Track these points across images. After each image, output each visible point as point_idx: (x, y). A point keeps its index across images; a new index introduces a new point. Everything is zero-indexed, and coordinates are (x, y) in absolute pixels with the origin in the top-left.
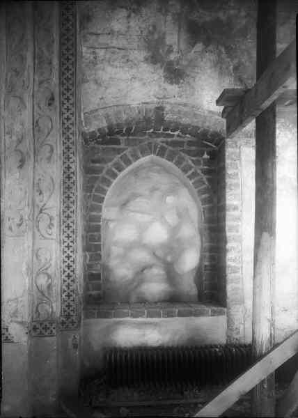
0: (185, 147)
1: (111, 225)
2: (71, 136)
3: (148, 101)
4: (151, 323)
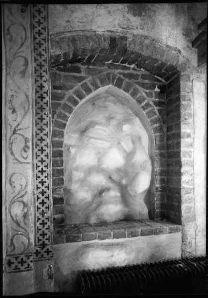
0: (140, 80)
1: (73, 150)
2: (43, 53)
3: (112, 29)
4: (118, 244)
